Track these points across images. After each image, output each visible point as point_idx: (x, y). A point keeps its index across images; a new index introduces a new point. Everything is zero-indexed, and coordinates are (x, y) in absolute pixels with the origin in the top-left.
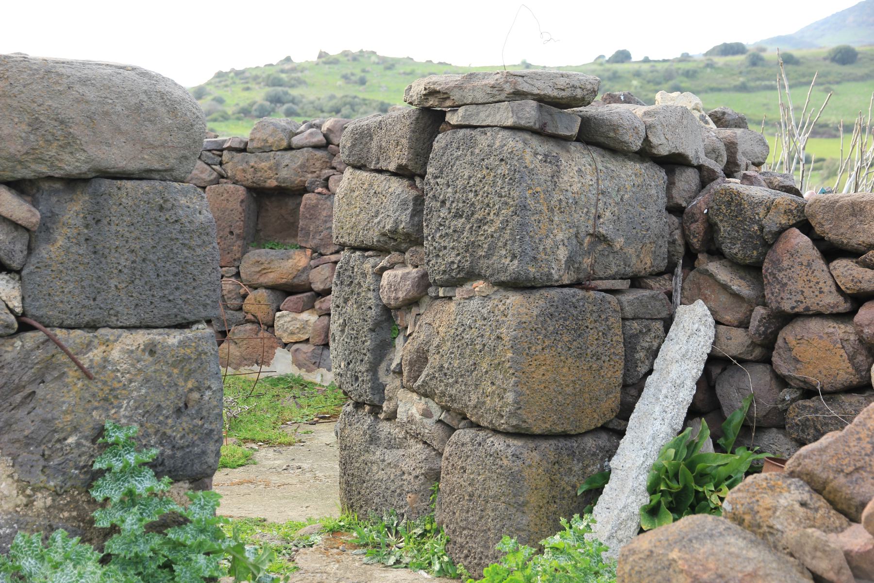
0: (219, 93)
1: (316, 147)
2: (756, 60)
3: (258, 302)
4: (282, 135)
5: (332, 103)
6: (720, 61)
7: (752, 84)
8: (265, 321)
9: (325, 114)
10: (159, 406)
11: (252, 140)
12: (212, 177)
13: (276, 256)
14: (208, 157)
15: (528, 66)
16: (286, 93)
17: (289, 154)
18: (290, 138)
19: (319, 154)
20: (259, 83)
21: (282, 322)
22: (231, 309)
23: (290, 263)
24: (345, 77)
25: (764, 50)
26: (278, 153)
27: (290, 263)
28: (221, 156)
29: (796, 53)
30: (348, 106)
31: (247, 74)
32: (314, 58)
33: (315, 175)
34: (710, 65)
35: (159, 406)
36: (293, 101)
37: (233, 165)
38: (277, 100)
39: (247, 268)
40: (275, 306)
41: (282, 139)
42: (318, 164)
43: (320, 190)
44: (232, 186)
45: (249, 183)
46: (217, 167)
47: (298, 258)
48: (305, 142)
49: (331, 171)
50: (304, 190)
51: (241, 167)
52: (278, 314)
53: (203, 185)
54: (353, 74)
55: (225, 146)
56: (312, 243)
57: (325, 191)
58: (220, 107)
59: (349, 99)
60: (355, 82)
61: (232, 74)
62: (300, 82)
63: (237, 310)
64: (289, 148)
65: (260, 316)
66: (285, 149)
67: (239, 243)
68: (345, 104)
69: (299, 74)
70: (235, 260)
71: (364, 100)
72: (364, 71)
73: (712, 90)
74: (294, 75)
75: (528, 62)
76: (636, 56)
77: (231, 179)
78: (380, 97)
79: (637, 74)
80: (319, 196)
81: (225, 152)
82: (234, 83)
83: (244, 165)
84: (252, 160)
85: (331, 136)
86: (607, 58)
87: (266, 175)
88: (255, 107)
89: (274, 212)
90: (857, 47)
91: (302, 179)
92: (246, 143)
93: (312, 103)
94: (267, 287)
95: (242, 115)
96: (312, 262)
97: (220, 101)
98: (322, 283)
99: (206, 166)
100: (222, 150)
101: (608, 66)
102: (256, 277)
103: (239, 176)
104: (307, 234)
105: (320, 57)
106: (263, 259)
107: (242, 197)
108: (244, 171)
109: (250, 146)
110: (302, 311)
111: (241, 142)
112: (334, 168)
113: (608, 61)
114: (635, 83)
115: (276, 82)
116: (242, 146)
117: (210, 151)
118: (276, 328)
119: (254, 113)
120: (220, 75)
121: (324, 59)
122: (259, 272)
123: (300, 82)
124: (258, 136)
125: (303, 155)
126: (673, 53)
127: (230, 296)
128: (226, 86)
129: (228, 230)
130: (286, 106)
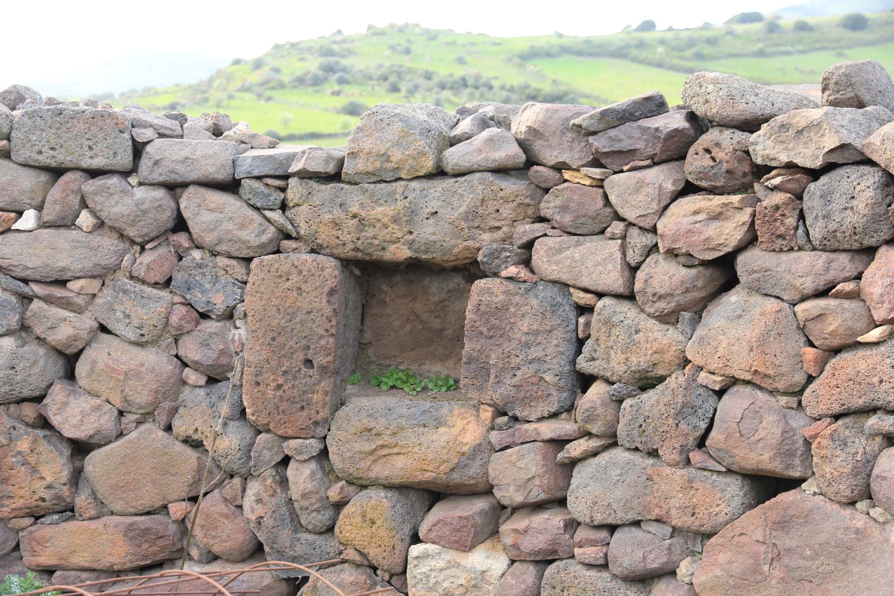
0: (275, 63)
1: (501, 171)
2: (773, 27)
3: (369, 520)
4: (421, 144)
5: (380, 72)
6: (740, 28)
7: (769, 50)
8: (385, 564)
9: (374, 82)
10: (212, 381)
11: (353, 154)
12: (265, 238)
13: (412, 417)
14: (256, 194)
15: (560, 36)
16: (337, 63)
17: (440, 186)
18: (441, 152)
19: (511, 186)
20: (312, 54)
21: (424, 569)
22: (308, 531)
23: (445, 433)
24: (392, 48)
25: (779, 18)
26: (414, 184)
27: (445, 433)
28: (283, 190)
29: (811, 20)
30: (395, 75)
31: (302, 46)
32: (364, 31)
33: (499, 235)
34: (730, 33)
35: (212, 381)
36: (344, 70)
37: (313, 210)
38: (329, 69)
39: (344, 448)
40: (407, 530)
41: (423, 154)
42: (507, 211)
43: (512, 270)
44: (310, 257)
45: (347, 251)
46: (276, 216)
47: (460, 424)
48: (477, 159)
49: (539, 228)
50: (471, 270)
51: (328, 217)
52: (416, 550)
53: (244, 253)
54: (399, 45)
55: (294, 168)
56: (498, 393)
57: (524, 273)
58: (277, 77)
59: (396, 68)
60: (401, 52)
61: (288, 46)
62: (350, 53)
63: (321, 533)
64: (440, 173)
65: (375, 554)
66: (429, 176)
67: (326, 384)
68: (392, 72)
69: (349, 46)
70: (316, 423)
71: (410, 68)
72: (409, 41)
73: (733, 55)
74: (345, 46)
75: (560, 32)
76: (661, 26)
77: (306, 241)
78: (423, 66)
79: (662, 42)
80: (511, 286)
81: (293, 181)
82: (289, 54)
83: (337, 213)
84: (355, 199)
85: (538, 146)
86: (634, 27)
87: (384, 234)
88: (309, 76)
89: (397, 306)
90: (868, 14)
91: (470, 243)
92: (341, 162)
93: (362, 71)
94: (388, 487)
95: (297, 84)
96: (494, 436)
97: (277, 70)
98: (519, 488)
99: (251, 213)
100: (286, 177)
101: (635, 35)
102: (363, 465)
103: (324, 236)
104: (484, 371)
105: (369, 28)
106: (379, 424)
107: (331, 283)
108: (336, 224)
109: (348, 168)
110: (471, 548)
111: (329, 158)
112: (542, 220)
113: (635, 30)
114: (660, 50)
115: (327, 52)
116: (331, 169)
117: (259, 178)
118: (410, 581)
119: (309, 82)
120: (277, 47)
121: (372, 31)
122: (372, 452)
123: (350, 53)
124: (367, 145)
125: (472, 190)
126: (695, 22)
127: (305, 503)
128: (283, 57)
129: (301, 356)
130: (338, 75)
